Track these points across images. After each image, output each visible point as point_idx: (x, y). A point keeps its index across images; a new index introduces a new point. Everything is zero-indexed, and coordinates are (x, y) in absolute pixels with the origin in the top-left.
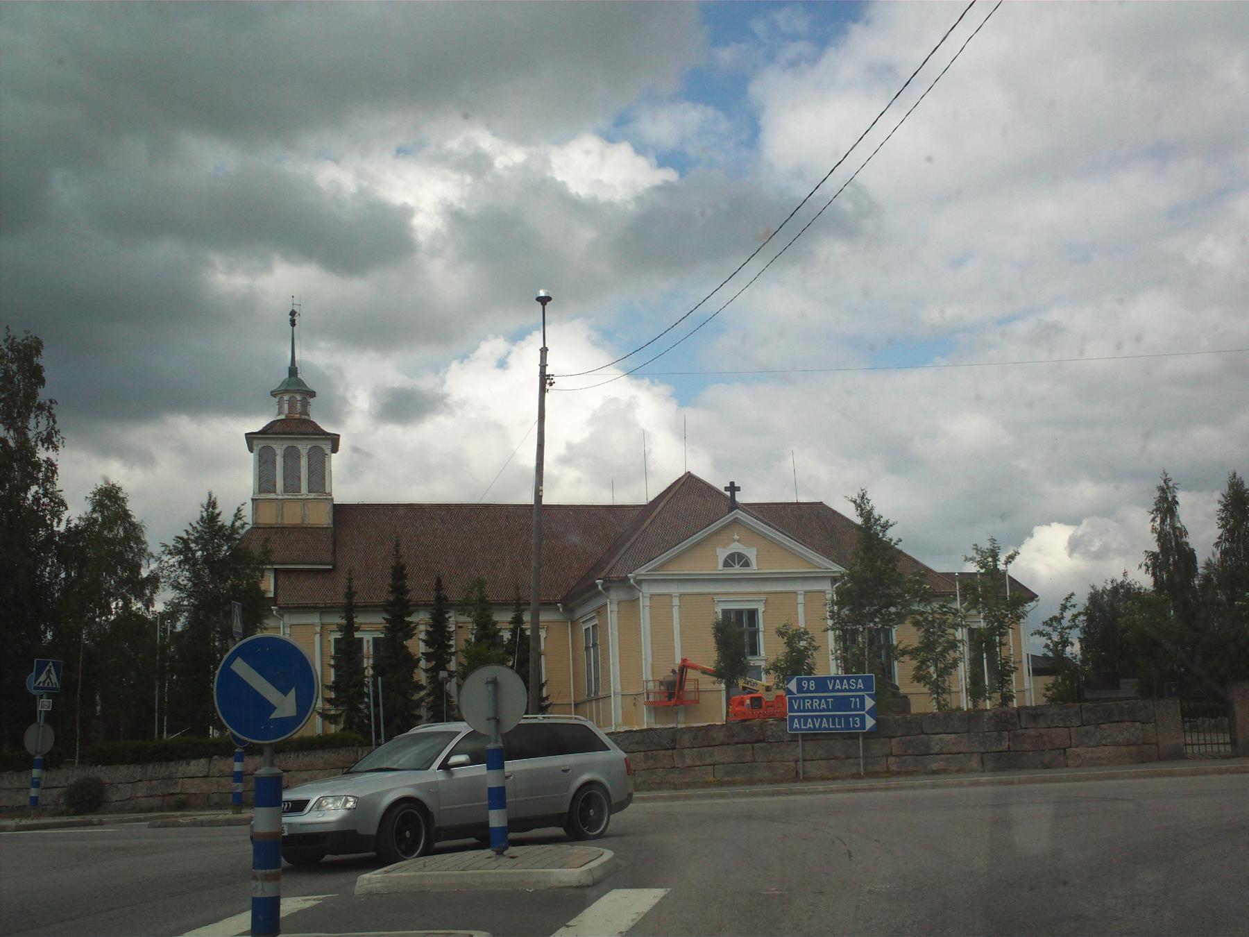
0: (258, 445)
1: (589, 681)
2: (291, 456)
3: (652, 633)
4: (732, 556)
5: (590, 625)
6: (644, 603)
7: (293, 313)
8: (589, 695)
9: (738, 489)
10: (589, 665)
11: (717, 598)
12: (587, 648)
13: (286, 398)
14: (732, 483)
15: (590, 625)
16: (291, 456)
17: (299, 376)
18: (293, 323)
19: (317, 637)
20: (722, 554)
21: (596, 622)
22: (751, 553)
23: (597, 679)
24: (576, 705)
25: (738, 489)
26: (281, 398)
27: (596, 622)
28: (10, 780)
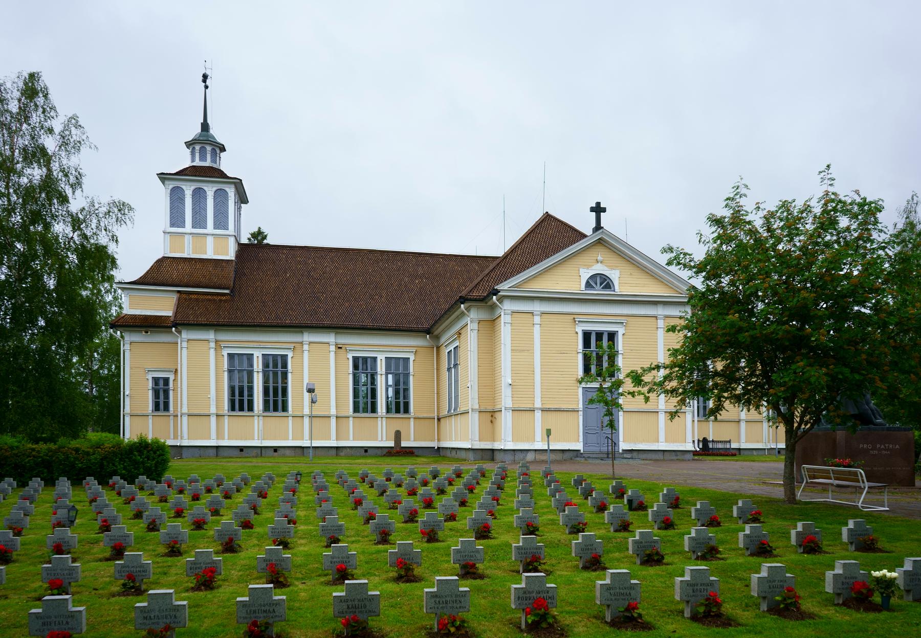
0: (171, 185)
1: (450, 385)
2: (199, 195)
3: (519, 272)
4: (593, 277)
5: (451, 348)
6: (505, 319)
7: (205, 77)
8: (449, 410)
9: (604, 210)
10: (450, 385)
11: (578, 318)
12: (449, 369)
13: (197, 147)
14: (598, 204)
15: (451, 348)
16: (199, 195)
17: (211, 131)
18: (204, 81)
19: (212, 352)
20: (586, 274)
21: (456, 344)
22: (614, 275)
23: (457, 397)
24: (439, 419)
25: (604, 210)
26: (194, 148)
27: (456, 344)
28: (2, 564)
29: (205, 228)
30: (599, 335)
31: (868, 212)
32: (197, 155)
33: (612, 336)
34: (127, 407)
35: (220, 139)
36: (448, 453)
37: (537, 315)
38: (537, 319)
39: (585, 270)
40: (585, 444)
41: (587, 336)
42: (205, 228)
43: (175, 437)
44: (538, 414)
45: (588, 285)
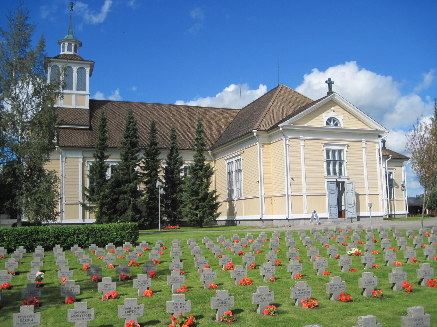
4: (329, 120)
22: (340, 118)
26: (64, 44)
29: (72, 90)
30: (334, 151)
31: (95, 215)
32: (66, 48)
33: (340, 151)
34: (13, 220)
35: (53, 170)
36: (396, 217)
37: (302, 140)
38: (302, 142)
39: (325, 115)
40: (330, 214)
41: (328, 151)
42: (72, 90)
43: (63, 51)
44: (305, 198)
45: (327, 124)
